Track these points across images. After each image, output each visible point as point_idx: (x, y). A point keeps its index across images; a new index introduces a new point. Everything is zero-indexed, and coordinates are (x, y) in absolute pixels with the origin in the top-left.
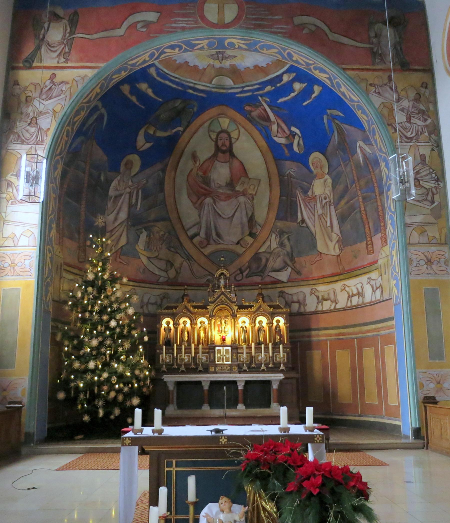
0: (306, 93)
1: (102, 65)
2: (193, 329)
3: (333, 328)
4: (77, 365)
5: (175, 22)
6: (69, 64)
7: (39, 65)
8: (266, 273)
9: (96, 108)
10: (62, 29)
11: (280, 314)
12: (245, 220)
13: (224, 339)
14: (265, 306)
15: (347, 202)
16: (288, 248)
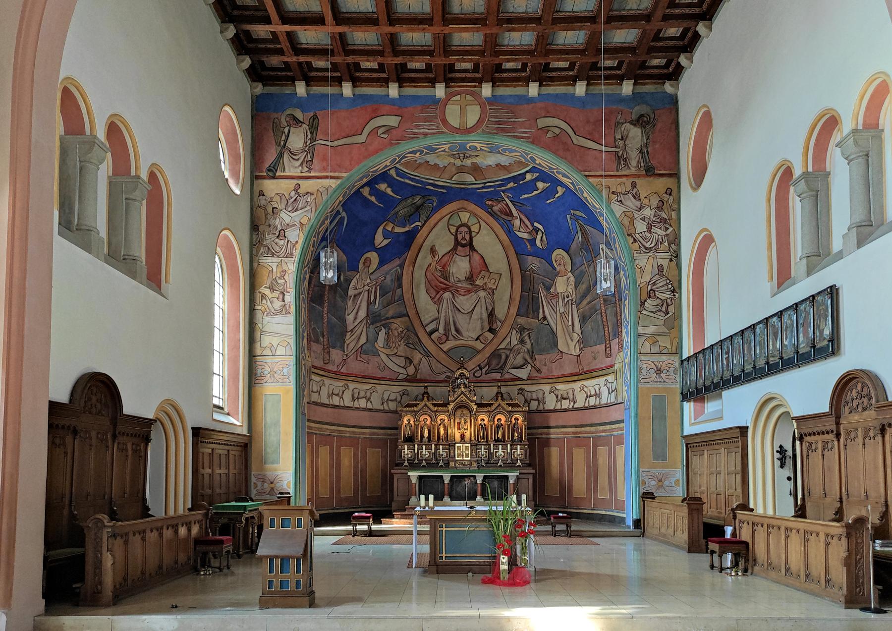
0: (549, 193)
3: (571, 427)
5: (417, 127)
6: (312, 174)
7: (282, 174)
9: (338, 213)
12: (485, 315)
15: (588, 303)
16: (529, 346)
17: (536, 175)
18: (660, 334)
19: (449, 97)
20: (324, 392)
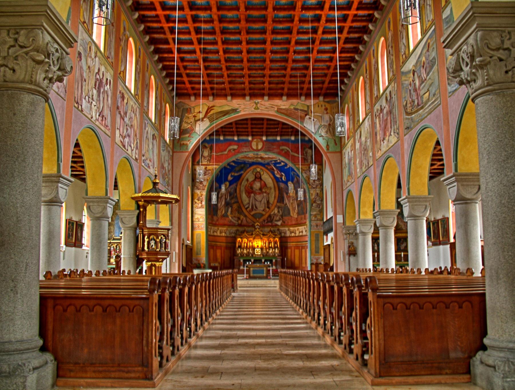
1: (221, 164)
8: (274, 221)
12: (266, 202)
13: (258, 246)
16: (281, 213)
19: (253, 139)
20: (212, 232)
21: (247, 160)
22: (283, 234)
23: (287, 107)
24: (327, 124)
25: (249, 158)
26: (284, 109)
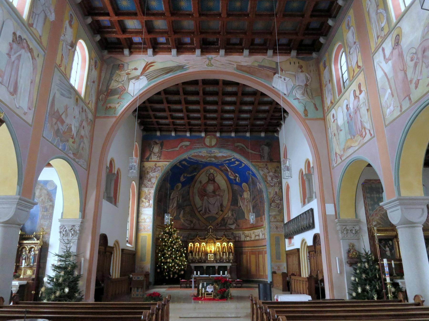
1: (171, 160)
2: (200, 247)
4: (163, 260)
10: (158, 148)
11: (231, 242)
12: (219, 205)
13: (211, 251)
14: (226, 239)
16: (235, 216)
17: (235, 160)
18: (276, 215)
21: (200, 159)
22: (237, 239)
23: (249, 64)
24: (303, 84)
25: (202, 156)
26: (245, 66)
